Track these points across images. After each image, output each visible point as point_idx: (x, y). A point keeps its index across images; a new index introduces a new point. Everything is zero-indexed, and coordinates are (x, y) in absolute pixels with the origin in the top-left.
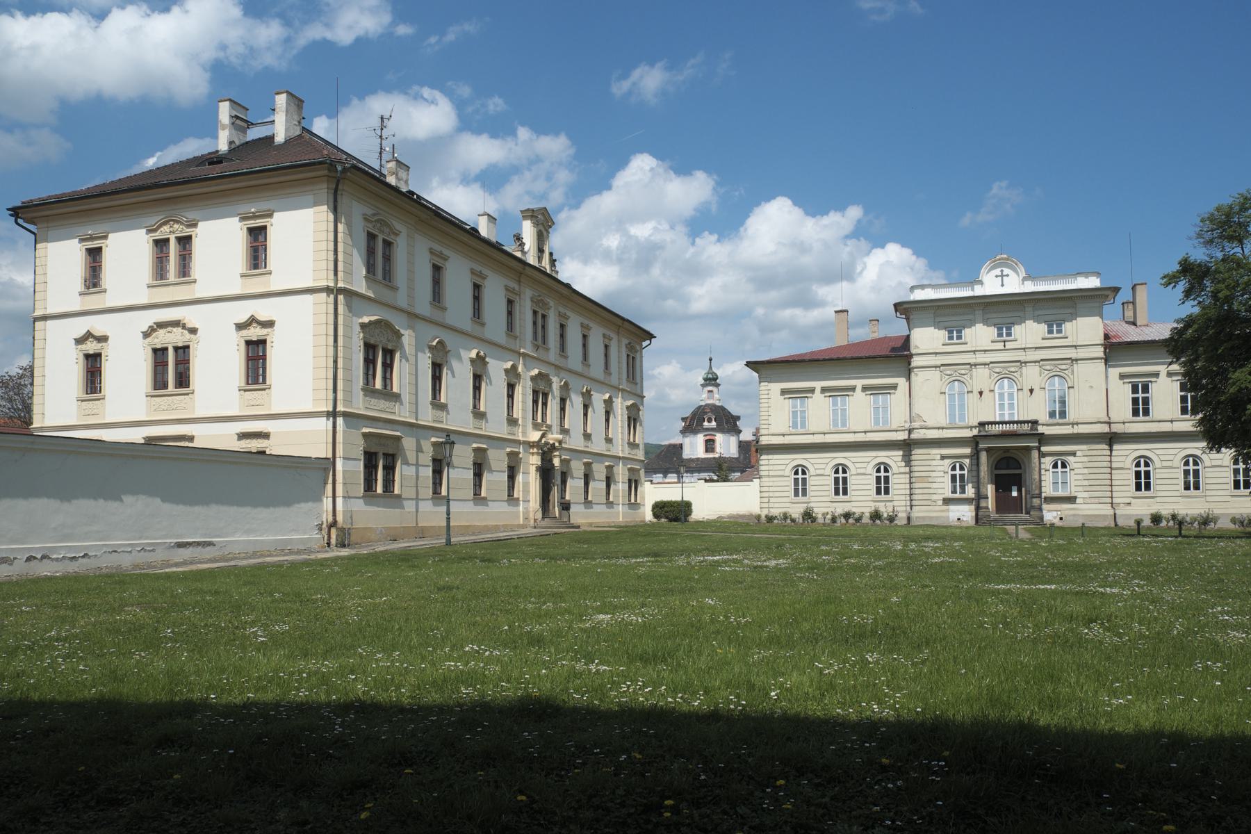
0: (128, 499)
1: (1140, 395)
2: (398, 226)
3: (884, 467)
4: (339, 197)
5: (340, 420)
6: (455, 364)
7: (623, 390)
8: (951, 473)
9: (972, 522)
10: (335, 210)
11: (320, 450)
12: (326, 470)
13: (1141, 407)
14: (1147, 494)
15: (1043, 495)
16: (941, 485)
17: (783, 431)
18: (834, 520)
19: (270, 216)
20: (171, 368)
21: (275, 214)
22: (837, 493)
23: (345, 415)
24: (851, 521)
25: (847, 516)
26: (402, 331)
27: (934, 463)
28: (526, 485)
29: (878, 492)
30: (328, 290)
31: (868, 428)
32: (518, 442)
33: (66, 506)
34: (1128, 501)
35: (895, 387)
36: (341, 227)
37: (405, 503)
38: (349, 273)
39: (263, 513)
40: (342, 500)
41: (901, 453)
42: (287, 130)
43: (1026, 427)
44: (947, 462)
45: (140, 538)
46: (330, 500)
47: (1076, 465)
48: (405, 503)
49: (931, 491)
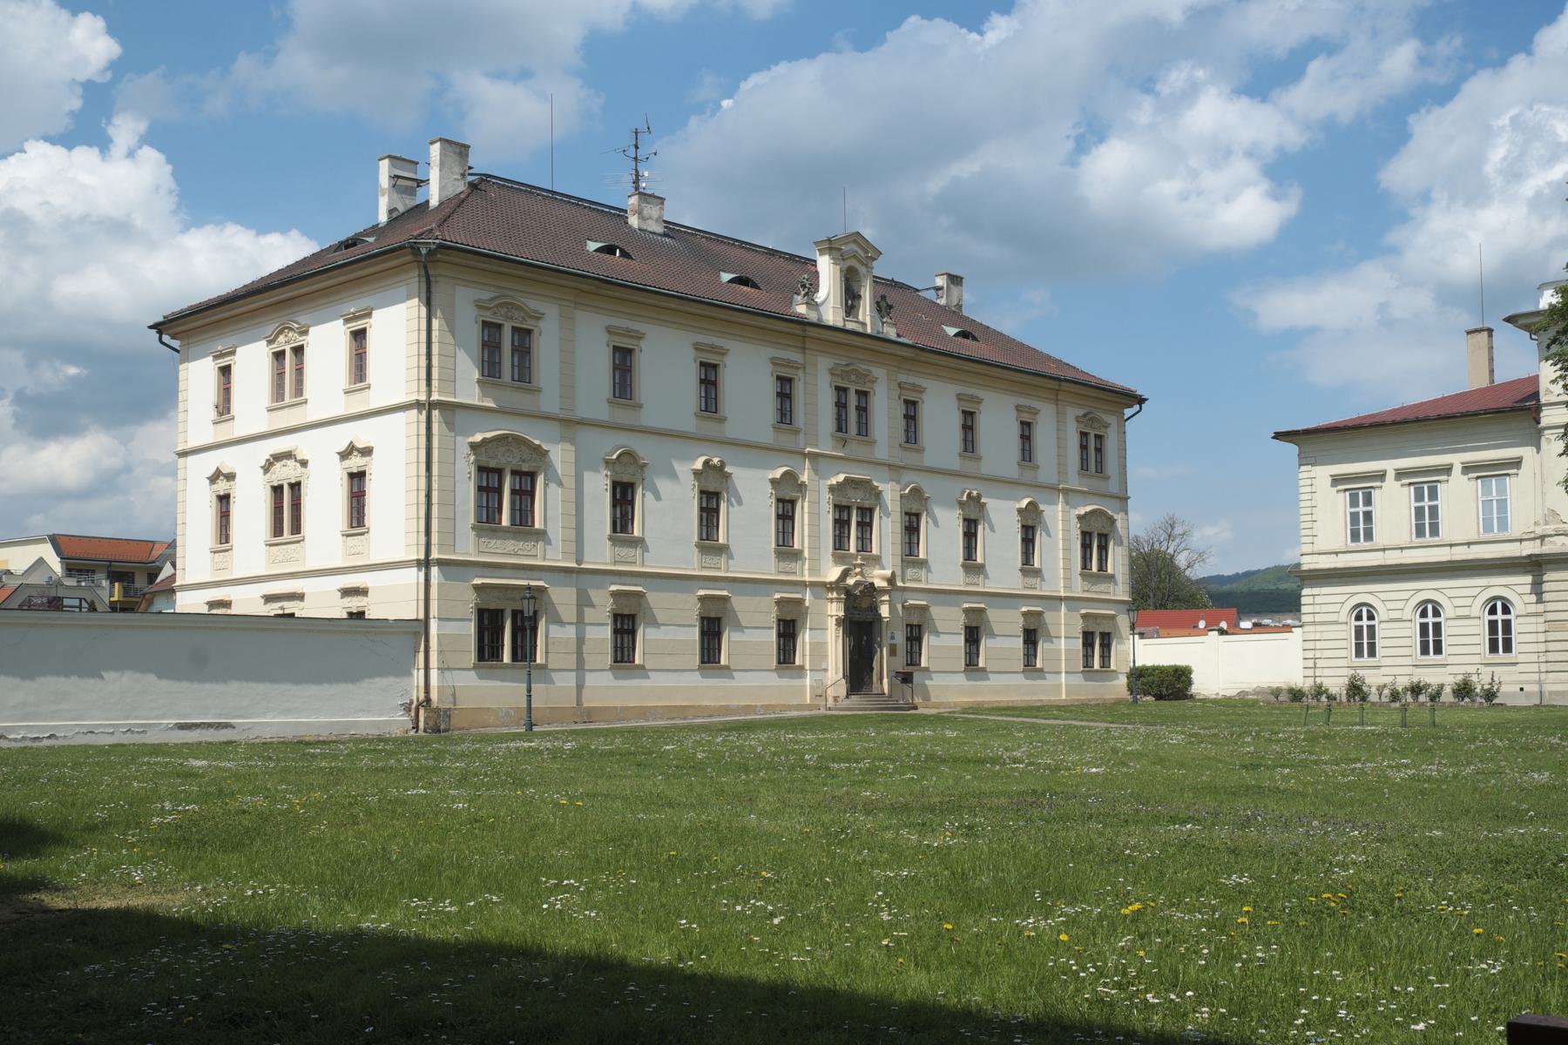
0: (108, 675)
2: (534, 304)
3: (1499, 605)
4: (433, 289)
5: (435, 571)
6: (663, 485)
7: (1066, 492)
8: (1488, 617)
10: (428, 304)
11: (410, 610)
12: (416, 634)
13: (1361, 527)
14: (1507, 658)
17: (1336, 547)
18: (1395, 696)
19: (369, 315)
20: (287, 508)
21: (312, 330)
22: (1425, 651)
23: (441, 563)
24: (1422, 698)
25: (1416, 690)
26: (545, 447)
28: (819, 649)
29: (1493, 648)
30: (418, 405)
31: (1473, 537)
32: (803, 584)
33: (27, 683)
35: (1517, 463)
36: (435, 323)
37: (554, 675)
38: (450, 381)
39: (312, 690)
40: (448, 673)
41: (1529, 579)
42: (441, 189)
45: (127, 718)
46: (422, 672)
48: (554, 675)
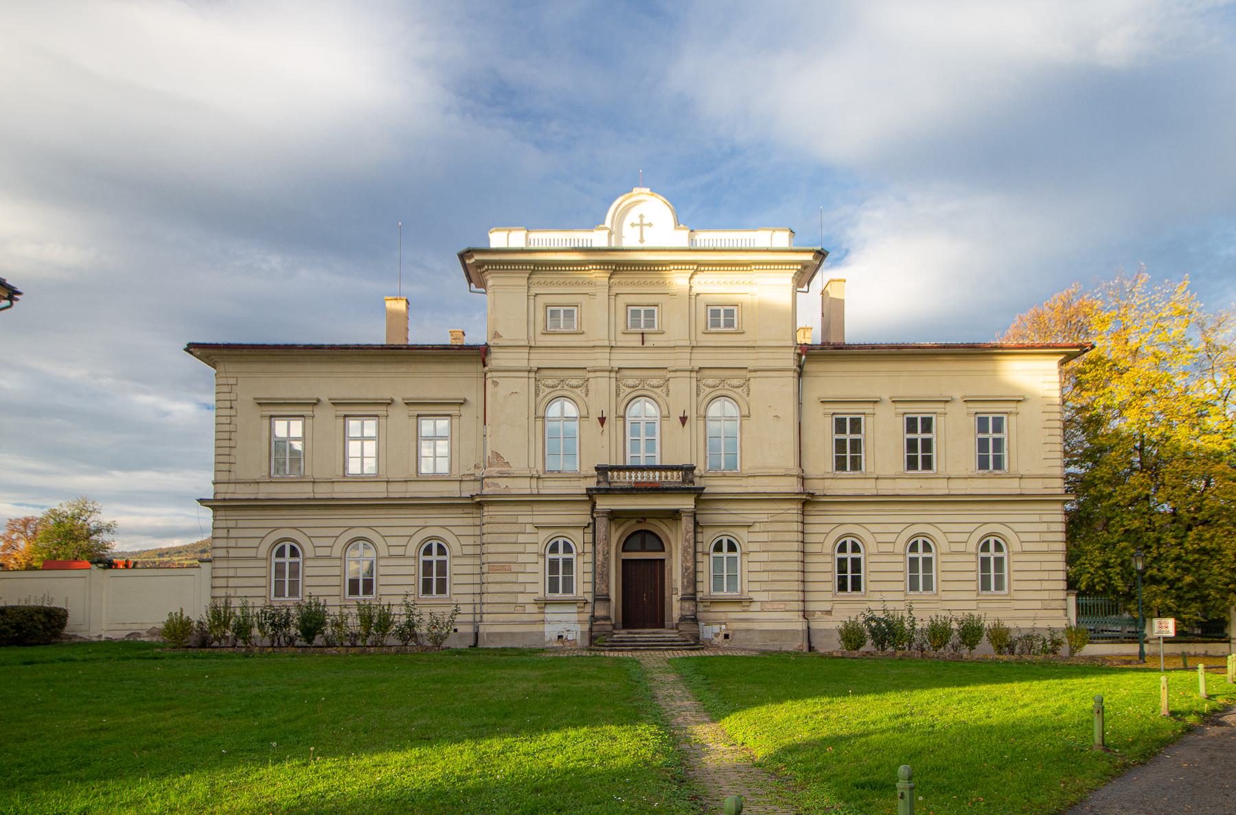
1: (991, 436)
9: (584, 642)
15: (699, 595)
16: (754, 577)
27: (522, 538)
34: (827, 607)
43: (675, 478)
44: (544, 535)
47: (752, 547)
49: (516, 588)
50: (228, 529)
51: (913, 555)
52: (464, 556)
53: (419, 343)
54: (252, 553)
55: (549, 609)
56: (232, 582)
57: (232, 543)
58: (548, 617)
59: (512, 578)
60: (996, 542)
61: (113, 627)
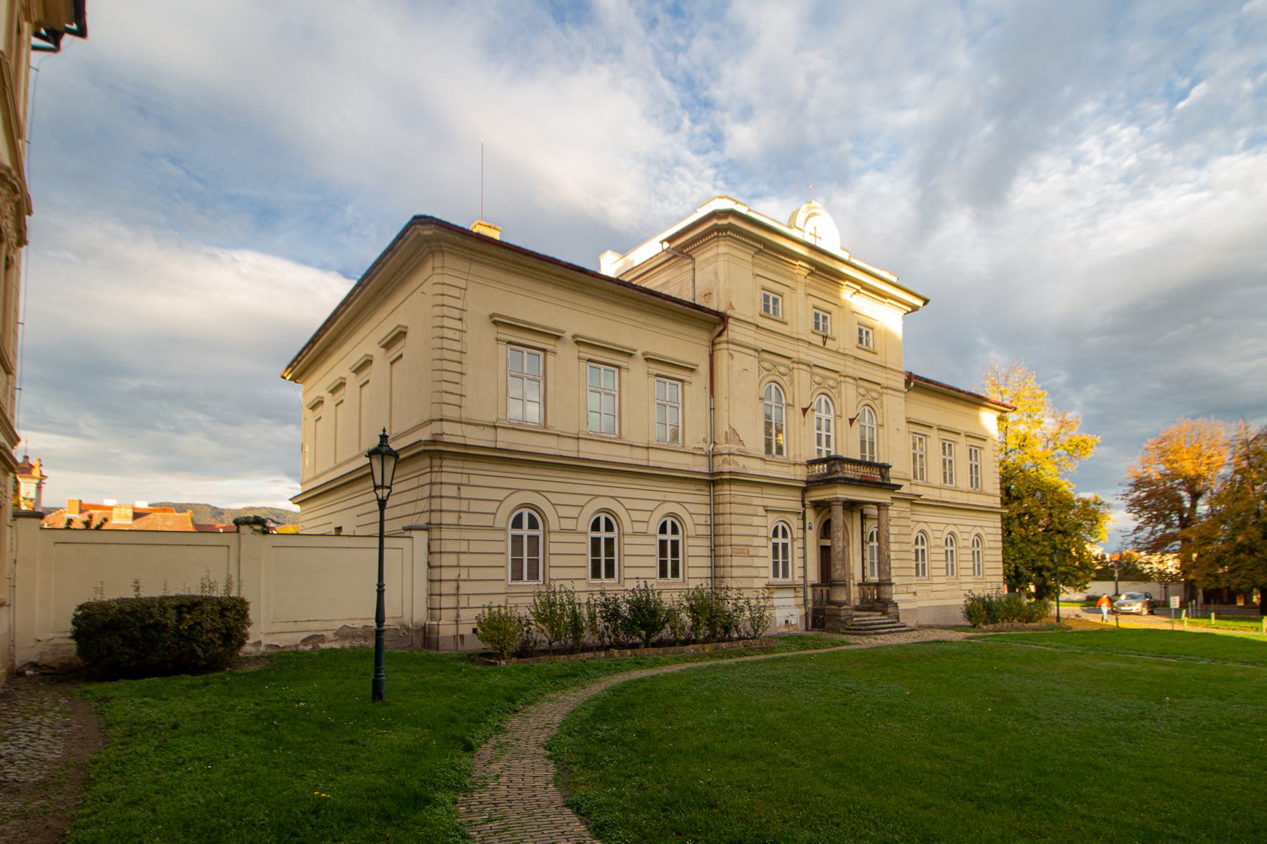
50: (459, 486)
51: (517, 532)
52: (698, 536)
53: (551, 255)
54: (487, 521)
55: (777, 594)
56: (465, 560)
57: (464, 506)
58: (776, 602)
59: (747, 561)
60: (530, 516)
61: (277, 628)
